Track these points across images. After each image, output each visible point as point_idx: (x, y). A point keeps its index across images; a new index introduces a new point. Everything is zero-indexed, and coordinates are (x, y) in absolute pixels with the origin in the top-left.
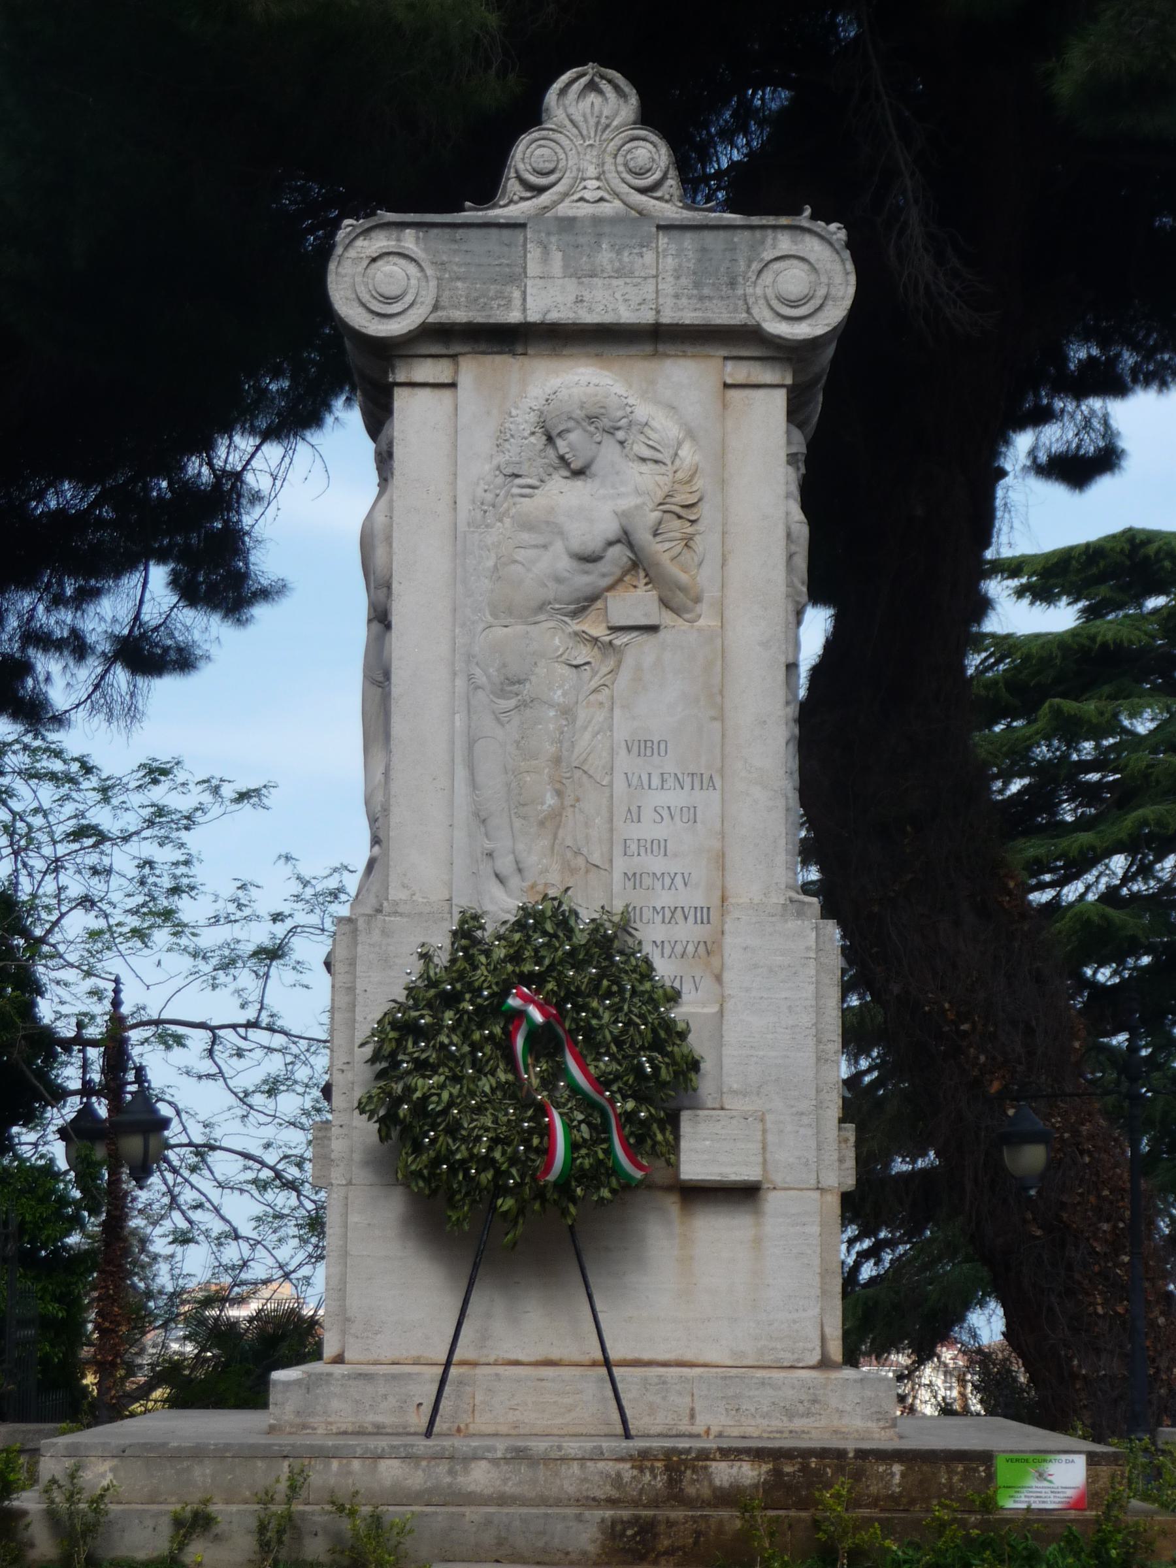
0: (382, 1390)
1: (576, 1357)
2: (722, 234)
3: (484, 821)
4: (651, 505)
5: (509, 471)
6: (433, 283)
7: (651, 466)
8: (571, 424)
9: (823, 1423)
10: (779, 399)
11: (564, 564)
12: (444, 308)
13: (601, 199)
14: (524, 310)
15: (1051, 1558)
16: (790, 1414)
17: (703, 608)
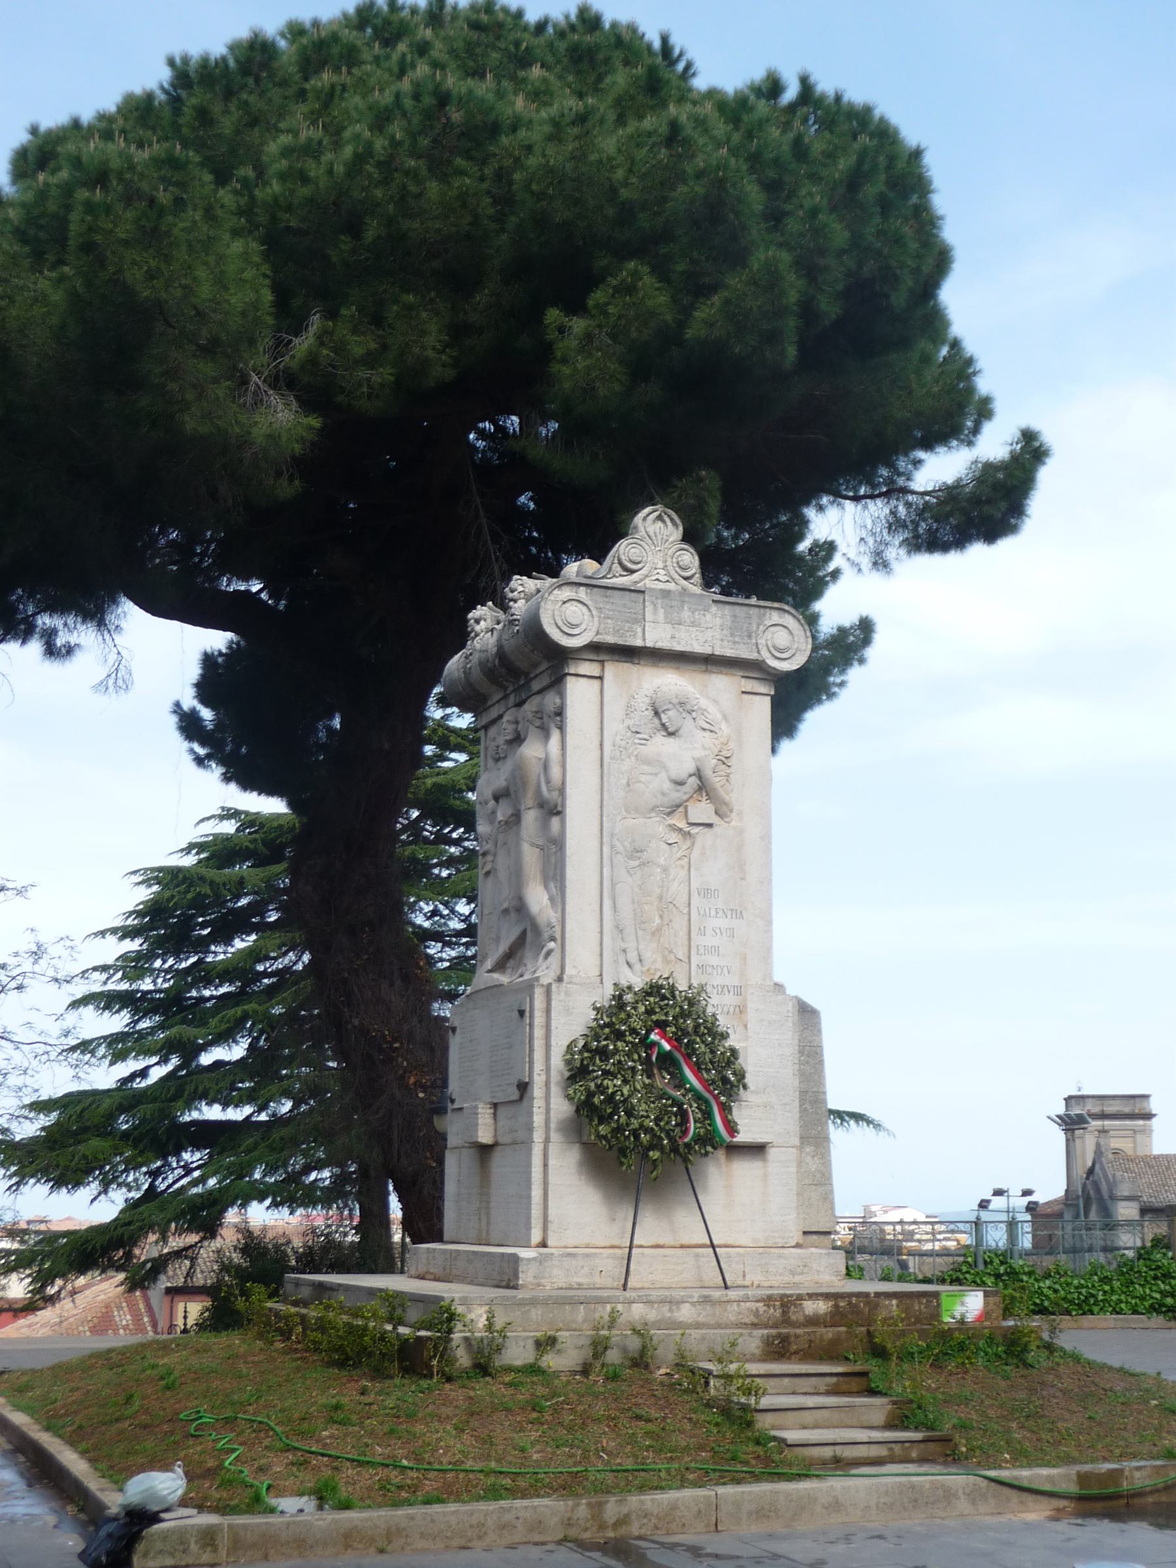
0: (581, 1264)
1: (672, 1243)
2: (744, 608)
3: (621, 931)
4: (712, 756)
5: (634, 730)
6: (596, 619)
7: (708, 733)
8: (670, 706)
9: (809, 1279)
10: (767, 701)
11: (667, 786)
12: (601, 634)
13: (668, 581)
14: (644, 640)
15: (120, 1357)
16: (793, 1273)
17: (734, 815)
